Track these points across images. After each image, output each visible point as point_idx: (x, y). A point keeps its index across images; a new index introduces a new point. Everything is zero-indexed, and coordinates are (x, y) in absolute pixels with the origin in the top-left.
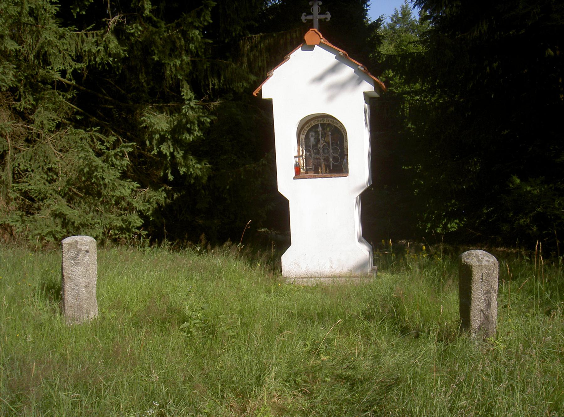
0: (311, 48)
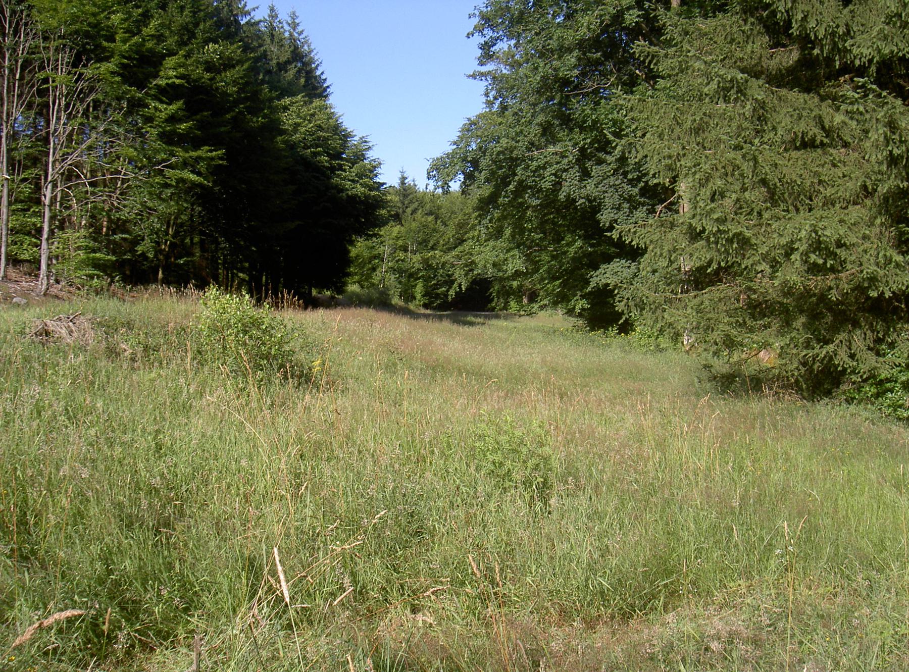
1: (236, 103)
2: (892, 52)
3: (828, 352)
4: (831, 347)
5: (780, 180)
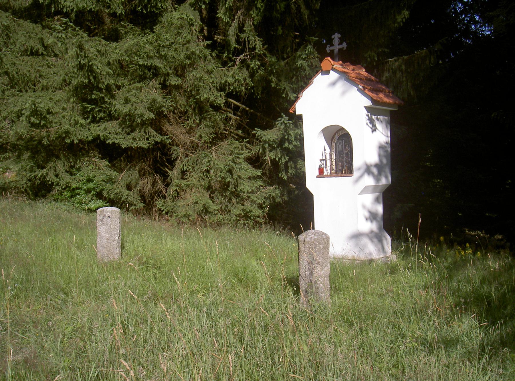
0: (327, 73)
2: (83, 7)
3: (43, 174)
4: (45, 171)
5: (17, 73)
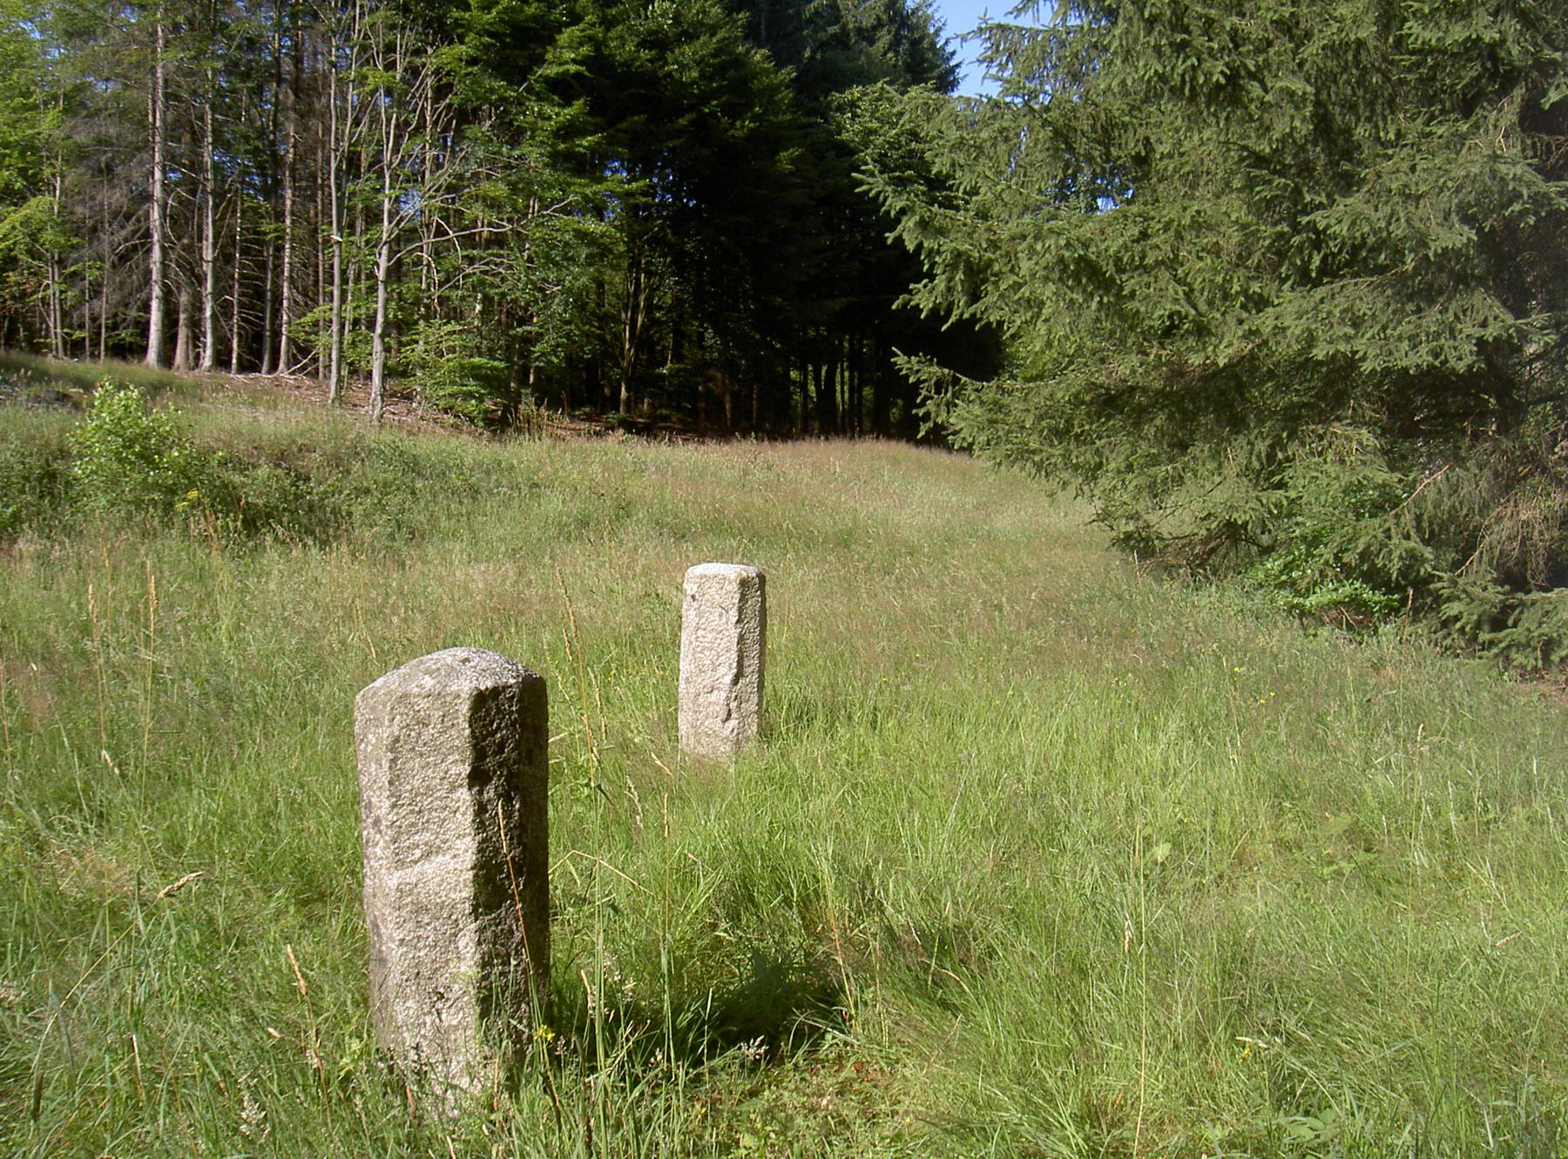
1: (704, 98)
